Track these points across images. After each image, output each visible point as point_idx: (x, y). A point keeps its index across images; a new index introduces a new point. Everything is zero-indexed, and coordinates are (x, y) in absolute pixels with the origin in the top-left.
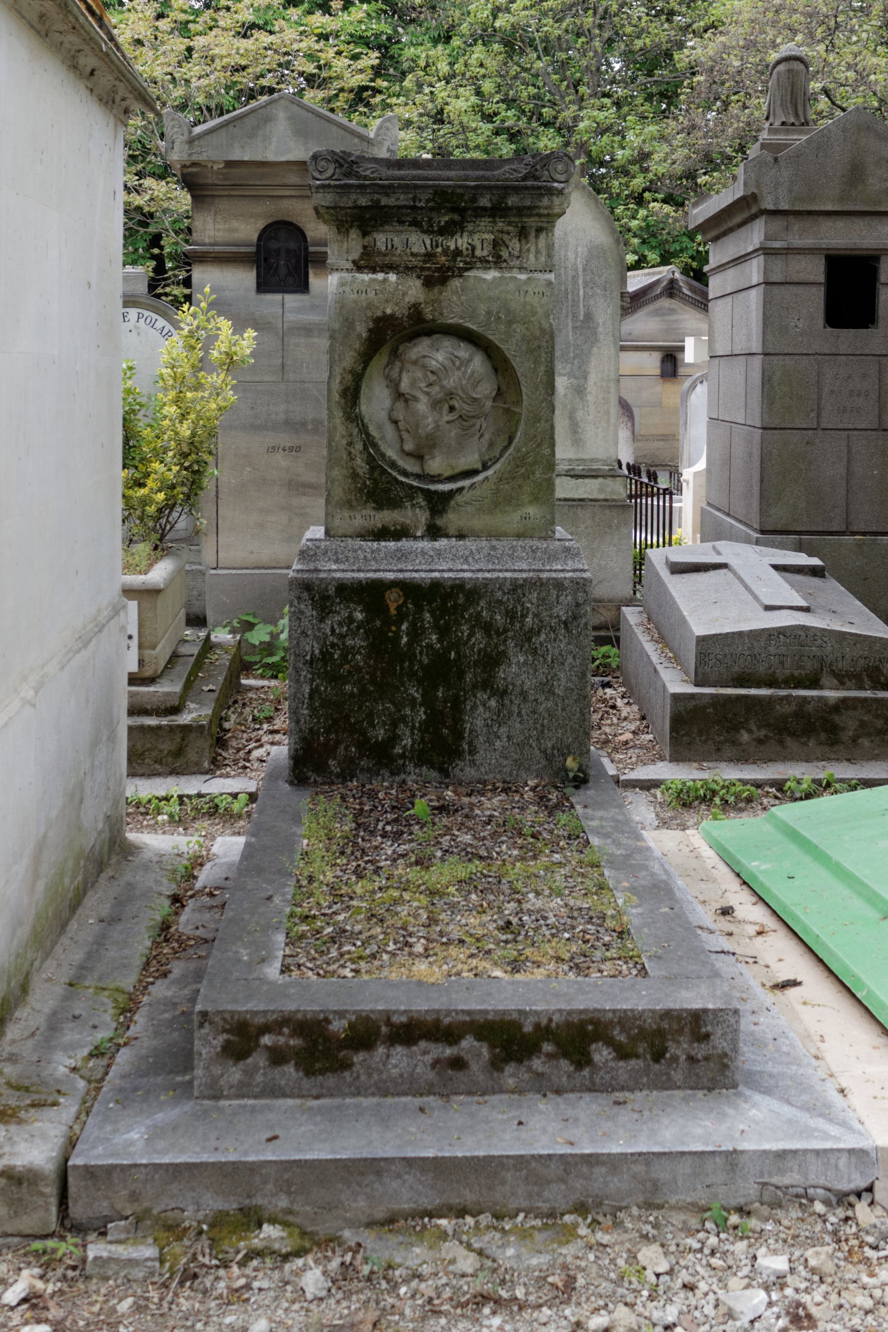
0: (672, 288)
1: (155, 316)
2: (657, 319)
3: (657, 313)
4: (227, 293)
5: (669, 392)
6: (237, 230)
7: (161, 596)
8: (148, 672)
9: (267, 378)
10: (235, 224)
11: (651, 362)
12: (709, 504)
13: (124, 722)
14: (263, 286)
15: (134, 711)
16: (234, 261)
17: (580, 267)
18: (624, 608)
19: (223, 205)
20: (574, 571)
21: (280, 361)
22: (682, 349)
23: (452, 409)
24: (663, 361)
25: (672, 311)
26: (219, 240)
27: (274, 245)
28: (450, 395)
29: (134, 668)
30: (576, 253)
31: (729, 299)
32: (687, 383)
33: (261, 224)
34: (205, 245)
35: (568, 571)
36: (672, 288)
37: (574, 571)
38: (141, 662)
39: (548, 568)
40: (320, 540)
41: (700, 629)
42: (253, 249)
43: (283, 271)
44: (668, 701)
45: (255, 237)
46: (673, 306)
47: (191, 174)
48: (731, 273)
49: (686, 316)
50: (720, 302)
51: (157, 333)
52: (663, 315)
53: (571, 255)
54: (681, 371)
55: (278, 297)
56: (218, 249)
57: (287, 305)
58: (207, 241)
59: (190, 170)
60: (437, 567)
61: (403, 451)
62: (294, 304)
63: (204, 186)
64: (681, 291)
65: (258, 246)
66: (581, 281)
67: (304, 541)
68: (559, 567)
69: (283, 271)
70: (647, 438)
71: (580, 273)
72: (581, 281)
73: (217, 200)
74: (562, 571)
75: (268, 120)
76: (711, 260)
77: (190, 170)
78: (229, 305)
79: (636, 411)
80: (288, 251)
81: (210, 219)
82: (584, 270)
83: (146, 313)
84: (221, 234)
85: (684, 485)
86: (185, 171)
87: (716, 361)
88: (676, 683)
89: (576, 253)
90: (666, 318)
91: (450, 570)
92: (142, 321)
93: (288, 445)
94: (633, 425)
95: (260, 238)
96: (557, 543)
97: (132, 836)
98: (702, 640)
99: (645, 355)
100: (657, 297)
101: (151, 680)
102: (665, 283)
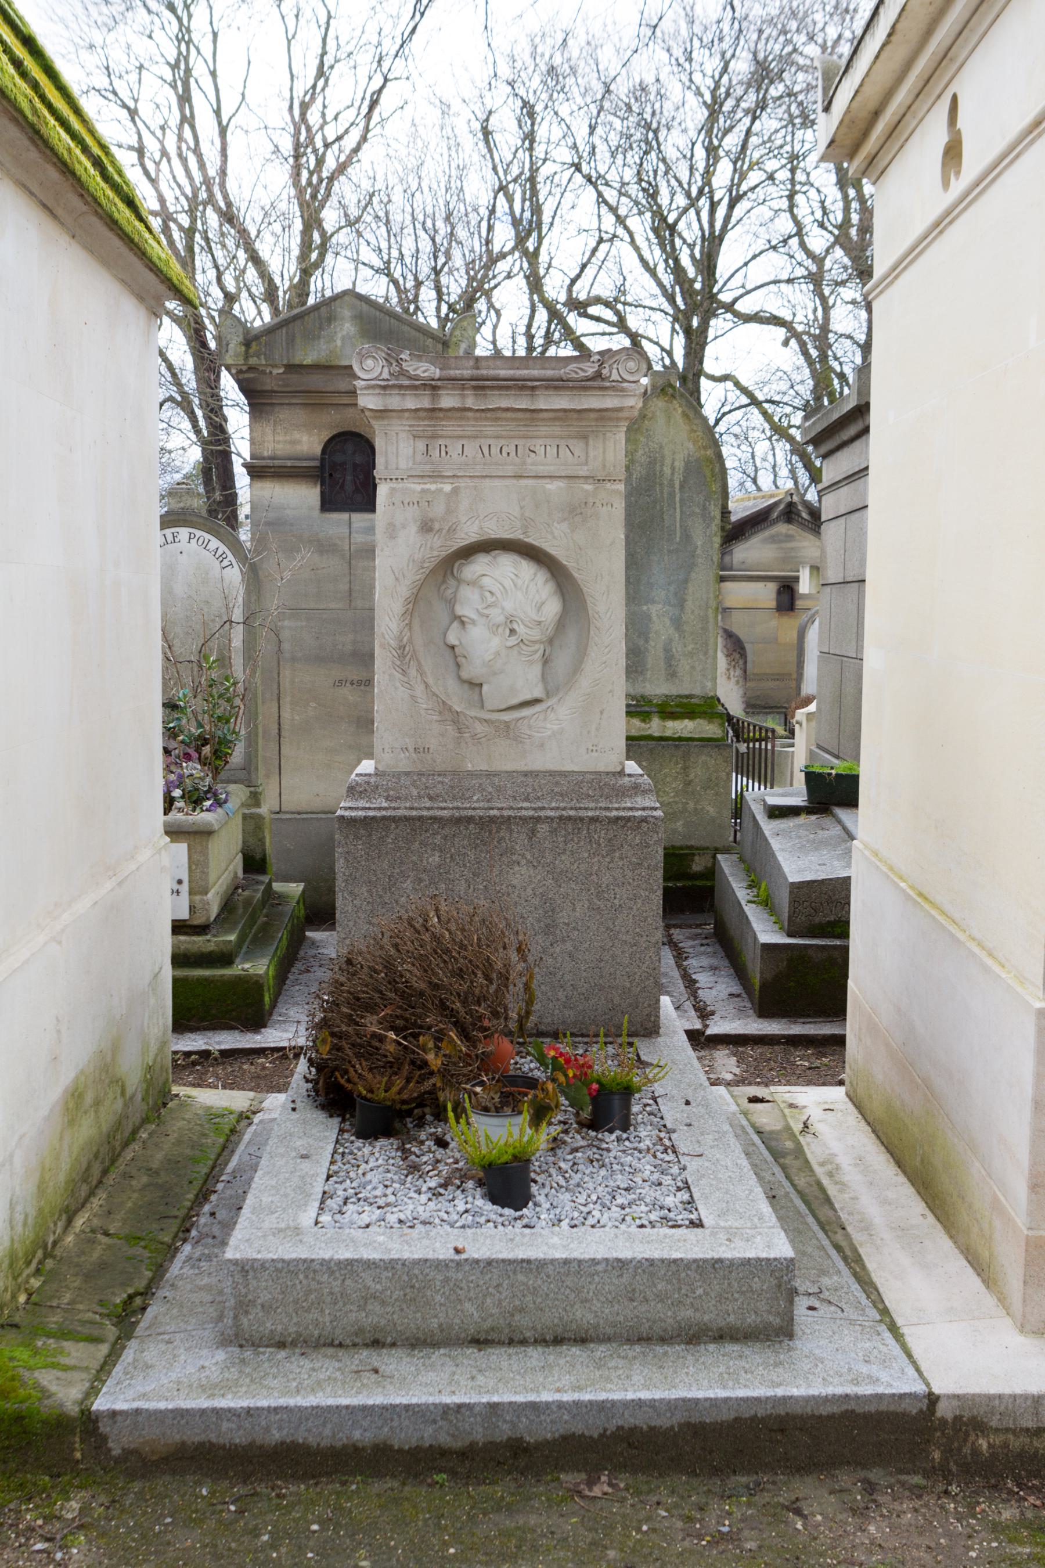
0: (790, 512)
1: (207, 536)
2: (774, 546)
3: (773, 539)
4: (288, 512)
5: (786, 628)
6: (299, 442)
7: (215, 837)
8: (198, 921)
9: (332, 605)
10: (297, 435)
11: (766, 594)
12: (819, 747)
13: (167, 973)
14: (328, 504)
15: (179, 960)
16: (297, 476)
17: (677, 486)
18: (719, 856)
19: (284, 414)
20: (644, 809)
21: (347, 587)
22: (797, 579)
23: (512, 631)
24: (779, 593)
25: (789, 538)
26: (278, 453)
27: (338, 458)
28: (510, 620)
29: (184, 914)
30: (673, 468)
31: (842, 520)
32: (804, 617)
33: (326, 435)
34: (264, 458)
35: (638, 809)
36: (790, 512)
37: (644, 809)
38: (192, 908)
39: (616, 805)
40: (370, 775)
41: (793, 878)
42: (317, 463)
43: (349, 487)
44: (758, 952)
45: (318, 450)
46: (791, 532)
47: (247, 380)
48: (844, 491)
49: (805, 544)
50: (833, 524)
51: (210, 555)
52: (780, 541)
53: (667, 471)
54: (799, 604)
55: (345, 516)
56: (277, 463)
57: (354, 526)
58: (266, 454)
59: (246, 376)
60: (494, 805)
61: (459, 678)
62: (362, 524)
63: (262, 393)
64: (800, 516)
65: (322, 460)
66: (677, 499)
67: (353, 776)
68: (629, 805)
69: (349, 487)
70: (761, 677)
71: (677, 490)
72: (677, 499)
73: (277, 409)
74: (631, 809)
75: (330, 319)
76: (824, 478)
77: (246, 376)
78: (292, 525)
79: (747, 646)
80: (355, 466)
81: (269, 430)
82: (682, 487)
83: (198, 533)
84: (280, 446)
85: (797, 727)
86: (241, 377)
87: (828, 589)
88: (767, 933)
89: (673, 468)
90: (783, 545)
91: (511, 808)
92: (194, 541)
93: (356, 678)
94: (745, 663)
95: (324, 452)
96: (627, 779)
97: (175, 1089)
98: (798, 888)
99: (759, 586)
100: (775, 522)
101: (202, 929)
102: (782, 506)
